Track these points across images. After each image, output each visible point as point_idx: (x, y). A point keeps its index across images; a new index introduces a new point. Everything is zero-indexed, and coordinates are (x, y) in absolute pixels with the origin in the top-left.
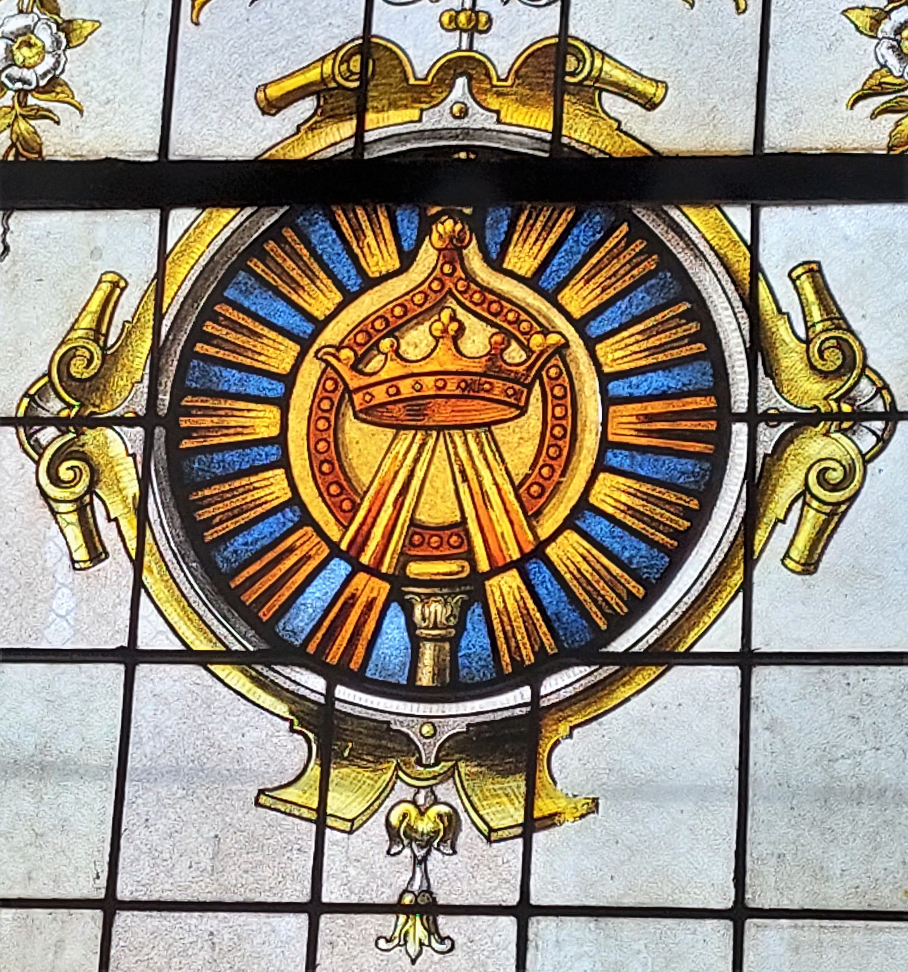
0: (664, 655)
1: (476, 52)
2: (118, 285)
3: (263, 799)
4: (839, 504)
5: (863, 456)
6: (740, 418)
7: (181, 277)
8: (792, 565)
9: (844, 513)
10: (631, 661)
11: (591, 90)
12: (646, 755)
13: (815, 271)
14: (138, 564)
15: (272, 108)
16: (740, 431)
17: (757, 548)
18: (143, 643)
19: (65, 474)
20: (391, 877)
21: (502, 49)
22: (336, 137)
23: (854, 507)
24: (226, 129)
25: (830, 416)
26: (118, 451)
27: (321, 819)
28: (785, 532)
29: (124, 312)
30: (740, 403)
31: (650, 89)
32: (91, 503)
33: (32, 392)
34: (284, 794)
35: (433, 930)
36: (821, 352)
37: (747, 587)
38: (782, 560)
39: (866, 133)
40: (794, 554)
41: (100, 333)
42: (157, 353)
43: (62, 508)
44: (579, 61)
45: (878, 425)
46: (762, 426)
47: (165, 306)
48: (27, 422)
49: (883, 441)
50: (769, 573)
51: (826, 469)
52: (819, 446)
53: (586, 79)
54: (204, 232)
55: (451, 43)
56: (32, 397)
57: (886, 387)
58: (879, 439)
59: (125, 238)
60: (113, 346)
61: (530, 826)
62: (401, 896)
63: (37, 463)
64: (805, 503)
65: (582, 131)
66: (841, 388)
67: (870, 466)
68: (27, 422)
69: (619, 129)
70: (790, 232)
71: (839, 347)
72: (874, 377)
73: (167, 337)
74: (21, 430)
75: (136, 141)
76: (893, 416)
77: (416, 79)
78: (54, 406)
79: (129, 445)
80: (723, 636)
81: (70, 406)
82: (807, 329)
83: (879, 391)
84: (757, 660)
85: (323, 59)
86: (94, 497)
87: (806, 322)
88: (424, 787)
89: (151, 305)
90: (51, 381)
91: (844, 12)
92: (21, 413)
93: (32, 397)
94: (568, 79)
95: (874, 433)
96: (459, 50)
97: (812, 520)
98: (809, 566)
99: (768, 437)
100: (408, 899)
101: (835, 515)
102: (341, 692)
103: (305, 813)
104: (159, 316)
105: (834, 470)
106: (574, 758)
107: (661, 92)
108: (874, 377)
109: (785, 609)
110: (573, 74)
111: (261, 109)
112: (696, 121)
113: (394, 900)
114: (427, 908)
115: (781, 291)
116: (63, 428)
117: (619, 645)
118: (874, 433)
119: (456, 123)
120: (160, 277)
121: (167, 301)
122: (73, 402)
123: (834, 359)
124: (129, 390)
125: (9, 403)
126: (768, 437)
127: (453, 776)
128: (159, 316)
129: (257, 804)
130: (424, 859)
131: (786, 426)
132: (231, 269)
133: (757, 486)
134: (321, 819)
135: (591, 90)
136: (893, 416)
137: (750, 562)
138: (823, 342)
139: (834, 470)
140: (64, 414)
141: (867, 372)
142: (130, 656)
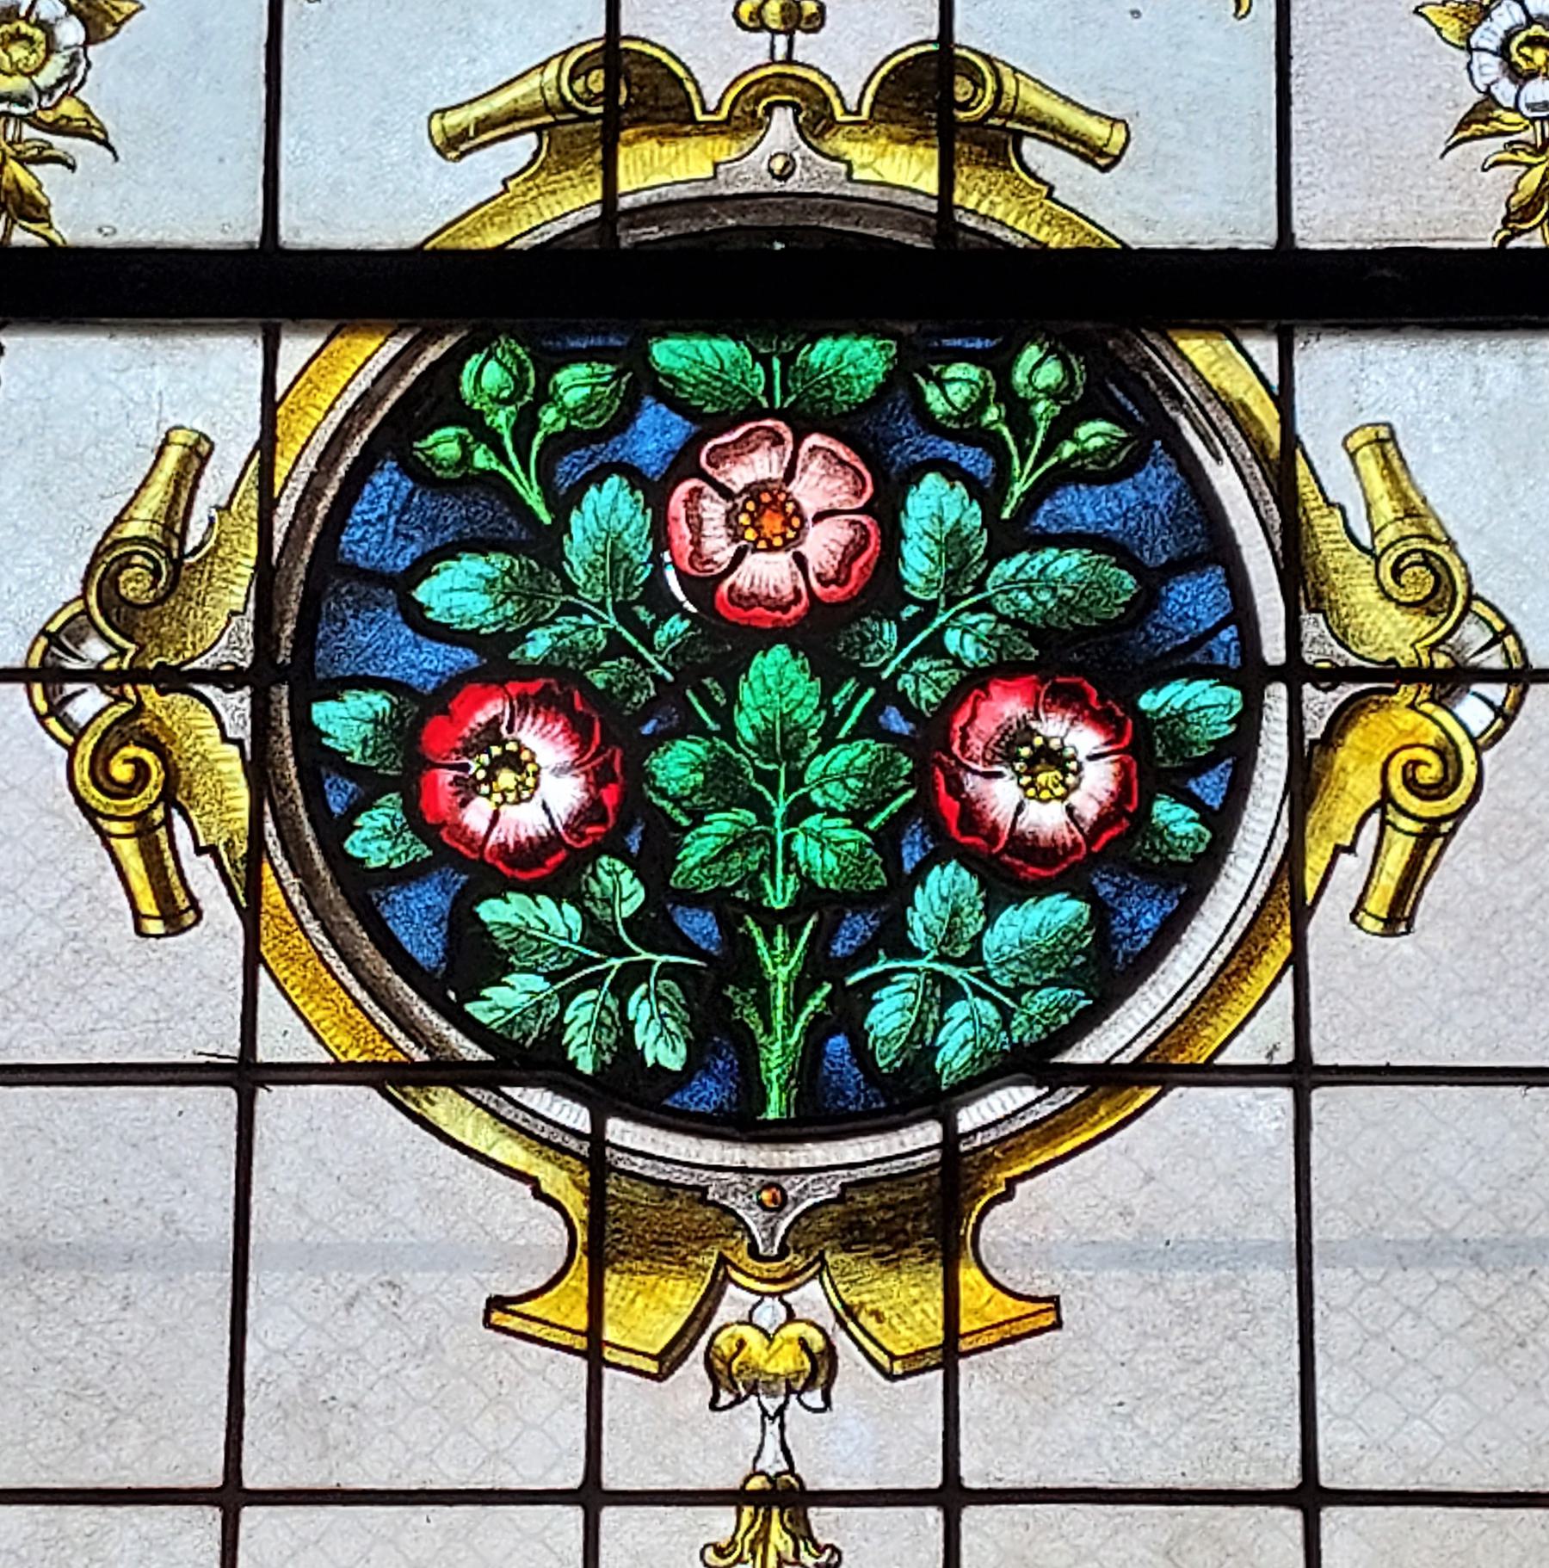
0: (1158, 1070)
1: (797, 63)
2: (198, 455)
3: (496, 1316)
4: (1436, 822)
5: (1473, 740)
6: (1276, 674)
7: (308, 427)
8: (1369, 923)
9: (1453, 831)
10: (1109, 1079)
11: (996, 141)
12: (1133, 1214)
13: (1385, 442)
14: (251, 916)
15: (454, 145)
16: (1277, 694)
17: (1311, 887)
18: (265, 1053)
19: (121, 772)
20: (729, 1447)
21: (847, 56)
22: (572, 202)
23: (1466, 823)
24: (375, 190)
25: (1415, 675)
26: (212, 735)
27: (594, 1352)
28: (1351, 869)
29: (213, 487)
30: (1274, 651)
31: (1097, 130)
32: (167, 822)
33: (53, 628)
34: (528, 1307)
35: (801, 1532)
36: (1396, 572)
37: (1297, 960)
38: (1353, 916)
39: (1459, 206)
40: (1371, 905)
41: (172, 531)
42: (266, 576)
43: (116, 827)
44: (975, 84)
45: (1496, 692)
46: (1308, 690)
47: (278, 482)
48: (47, 675)
49: (1505, 716)
50: (1328, 924)
51: (1416, 763)
52: (1403, 723)
53: (991, 113)
54: (338, 371)
55: (754, 50)
56: (54, 639)
57: (1510, 629)
58: (1498, 712)
59: (207, 379)
60: (196, 550)
61: (949, 1355)
62: (747, 1480)
63: (72, 750)
64: (1384, 823)
65: (987, 202)
66: (1435, 630)
67: (1487, 757)
68: (47, 675)
69: (1049, 196)
70: (1351, 382)
71: (1426, 563)
72: (1489, 614)
73: (281, 555)
74: (37, 688)
75: (221, 219)
76: (1522, 676)
77: (705, 111)
78: (95, 650)
79: (200, 831)
80: (1266, 1036)
81: (122, 652)
82: (1374, 535)
83: (1497, 638)
84: (1322, 1077)
85: (545, 64)
86: (174, 811)
87: (1371, 526)
88: (772, 1295)
89: (253, 500)
90: (86, 611)
91: (1416, 11)
92: (35, 662)
93: (54, 639)
94: (961, 115)
95: (1490, 704)
96: (773, 62)
97: (1399, 852)
98: (1398, 919)
99: (1320, 704)
100: (756, 1484)
101: (1431, 834)
102: (618, 1130)
103: (566, 1339)
104: (268, 504)
105: (1428, 765)
106: (1022, 1228)
107: (1119, 137)
108: (1489, 614)
109: (1365, 991)
110: (965, 107)
111: (438, 150)
112: (1183, 195)
113: (736, 1484)
114: (785, 1497)
115: (1334, 473)
116: (115, 691)
117: (1091, 1050)
118: (1490, 704)
119: (777, 185)
120: (267, 446)
121: (282, 466)
122: (127, 645)
123: (1418, 584)
124: (221, 622)
125: (10, 647)
126: (1320, 704)
127: (727, 1277)
128: (268, 504)
129: (1055, 1300)
130: (780, 1411)
131: (1347, 690)
132: (396, 427)
133: (1304, 787)
134: (594, 1352)
135: (996, 141)
136: (1522, 676)
137: (1301, 913)
138: (1401, 558)
139: (1428, 765)
140: (111, 665)
141: (1477, 606)
142: (246, 1075)
